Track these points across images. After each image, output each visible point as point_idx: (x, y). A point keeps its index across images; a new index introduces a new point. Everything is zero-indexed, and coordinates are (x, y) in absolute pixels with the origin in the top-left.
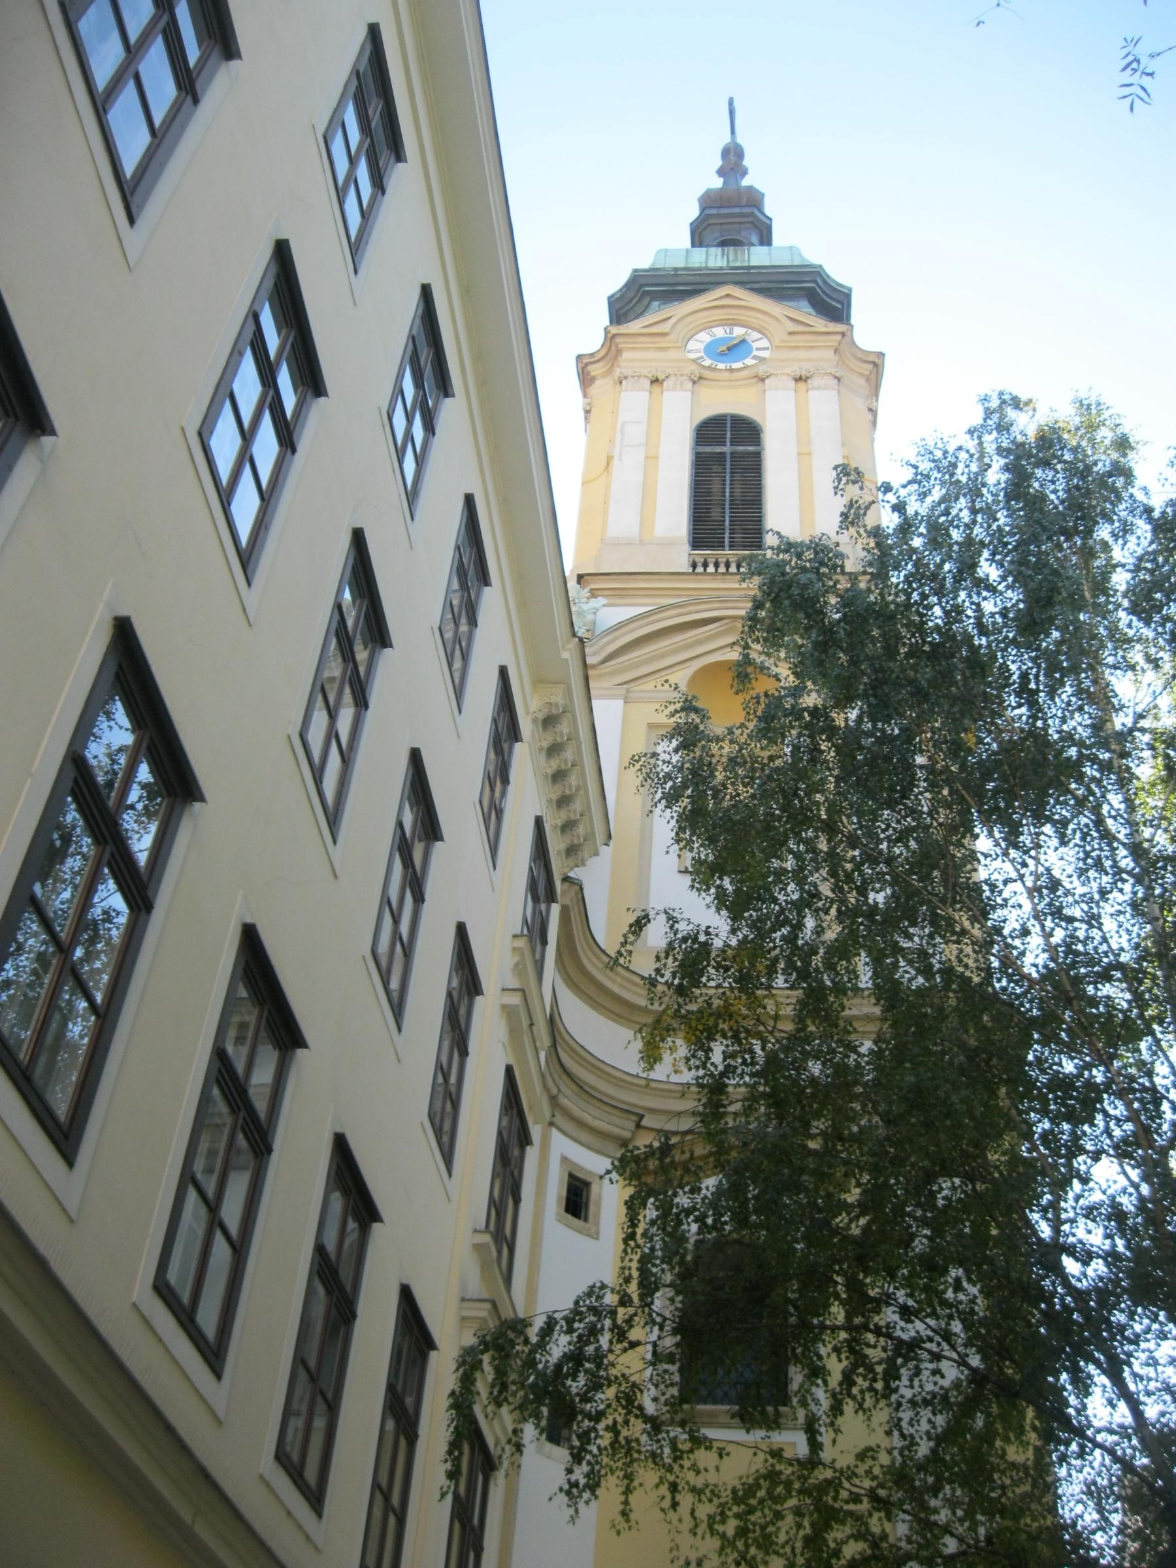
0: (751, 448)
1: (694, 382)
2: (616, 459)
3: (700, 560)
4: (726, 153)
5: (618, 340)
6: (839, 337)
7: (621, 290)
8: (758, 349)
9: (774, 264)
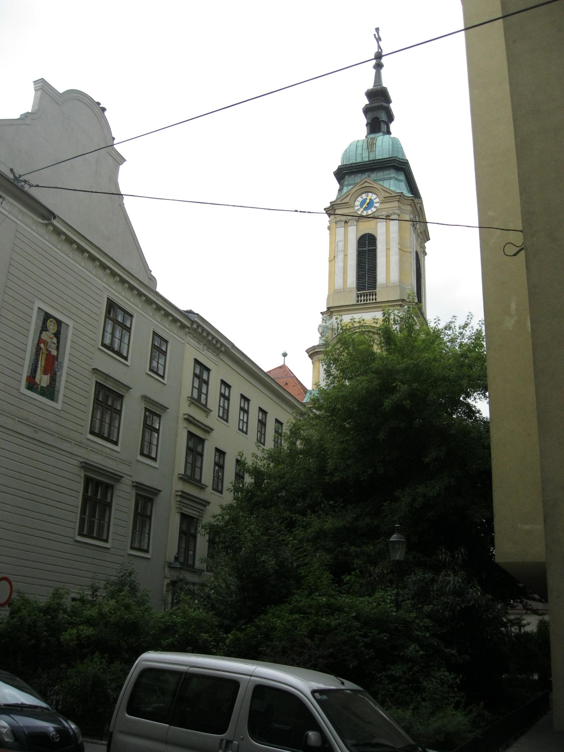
0: (373, 248)
1: (357, 221)
2: (336, 257)
3: (360, 295)
4: (370, 94)
5: (334, 206)
6: (399, 197)
7: (338, 169)
8: (376, 203)
9: (383, 158)
